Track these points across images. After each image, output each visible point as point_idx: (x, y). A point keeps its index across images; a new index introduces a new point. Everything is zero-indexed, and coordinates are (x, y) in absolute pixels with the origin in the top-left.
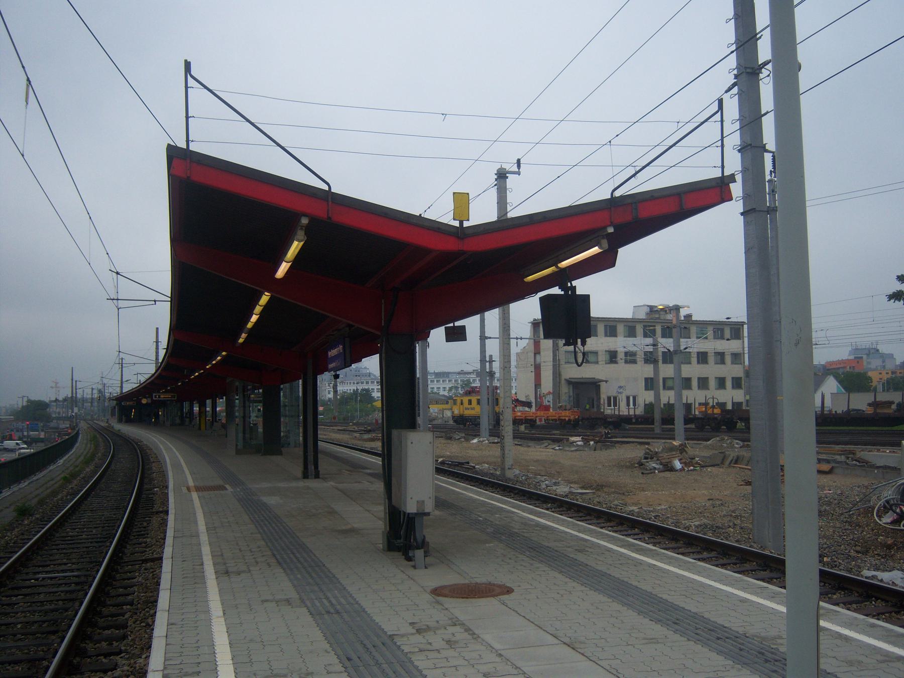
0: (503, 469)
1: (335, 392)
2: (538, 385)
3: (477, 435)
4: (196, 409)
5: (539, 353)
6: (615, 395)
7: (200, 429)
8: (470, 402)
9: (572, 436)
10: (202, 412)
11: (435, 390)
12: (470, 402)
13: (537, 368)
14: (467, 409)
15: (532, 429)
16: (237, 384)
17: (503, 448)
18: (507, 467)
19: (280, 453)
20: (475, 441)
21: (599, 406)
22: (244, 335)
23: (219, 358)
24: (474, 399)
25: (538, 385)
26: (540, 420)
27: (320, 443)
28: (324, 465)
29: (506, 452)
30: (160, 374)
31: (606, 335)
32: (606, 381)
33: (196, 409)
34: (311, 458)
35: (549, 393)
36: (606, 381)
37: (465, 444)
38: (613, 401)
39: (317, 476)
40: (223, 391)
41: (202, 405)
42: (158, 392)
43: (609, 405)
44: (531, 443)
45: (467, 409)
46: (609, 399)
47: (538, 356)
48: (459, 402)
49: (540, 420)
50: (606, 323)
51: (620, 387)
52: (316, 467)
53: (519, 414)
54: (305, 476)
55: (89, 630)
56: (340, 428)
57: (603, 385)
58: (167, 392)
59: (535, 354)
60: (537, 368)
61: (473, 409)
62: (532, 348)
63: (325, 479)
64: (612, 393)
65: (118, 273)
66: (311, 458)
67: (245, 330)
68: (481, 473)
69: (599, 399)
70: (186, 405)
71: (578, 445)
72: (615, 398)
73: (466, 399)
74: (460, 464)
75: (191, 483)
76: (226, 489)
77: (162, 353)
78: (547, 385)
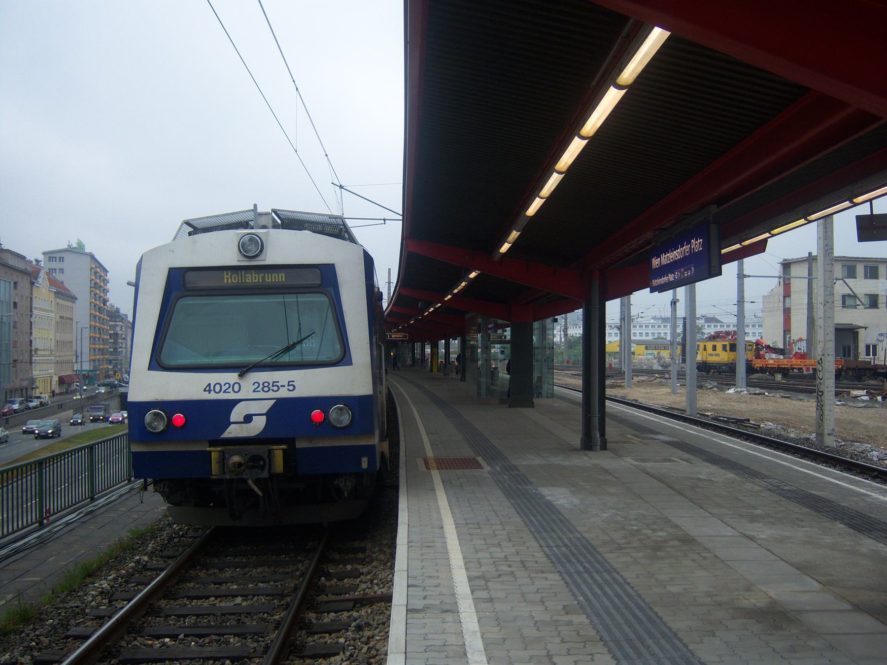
0: (820, 435)
1: (566, 335)
2: (787, 330)
3: (730, 385)
4: (428, 350)
5: (789, 296)
6: (874, 342)
7: (431, 371)
8: (714, 348)
9: (853, 389)
10: (435, 353)
11: (662, 335)
12: (714, 348)
13: (787, 312)
14: (711, 355)
15: (794, 378)
16: (480, 321)
17: (820, 407)
18: (826, 432)
19: (532, 405)
20: (731, 391)
21: (857, 355)
22: (449, 297)
23: (463, 284)
24: (719, 345)
25: (787, 330)
26: (808, 370)
27: (608, 403)
28: (611, 431)
29: (826, 412)
30: (391, 310)
31: (866, 277)
32: (866, 328)
33: (428, 350)
34: (596, 421)
35: (801, 340)
36: (866, 328)
37: (721, 394)
38: (872, 349)
39: (604, 447)
40: (461, 332)
41: (435, 347)
42: (390, 331)
43: (868, 354)
44: (801, 396)
45: (711, 355)
46: (868, 347)
47: (787, 299)
48: (702, 347)
49: (808, 370)
50: (867, 264)
51: (881, 335)
52: (603, 434)
53: (771, 362)
54: (588, 445)
55: (312, 616)
56: (573, 372)
57: (861, 332)
58: (399, 331)
59: (784, 297)
60: (787, 312)
61: (717, 355)
62: (781, 290)
63: (618, 454)
64: (872, 341)
65: (341, 187)
66: (596, 421)
67: (522, 222)
68: (769, 432)
69: (857, 347)
70: (418, 345)
71: (863, 401)
72: (875, 347)
73: (709, 345)
74: (738, 422)
75: (430, 454)
76: (481, 467)
77: (392, 290)
78: (799, 329)
